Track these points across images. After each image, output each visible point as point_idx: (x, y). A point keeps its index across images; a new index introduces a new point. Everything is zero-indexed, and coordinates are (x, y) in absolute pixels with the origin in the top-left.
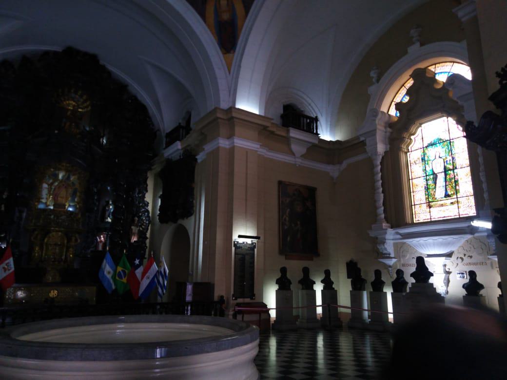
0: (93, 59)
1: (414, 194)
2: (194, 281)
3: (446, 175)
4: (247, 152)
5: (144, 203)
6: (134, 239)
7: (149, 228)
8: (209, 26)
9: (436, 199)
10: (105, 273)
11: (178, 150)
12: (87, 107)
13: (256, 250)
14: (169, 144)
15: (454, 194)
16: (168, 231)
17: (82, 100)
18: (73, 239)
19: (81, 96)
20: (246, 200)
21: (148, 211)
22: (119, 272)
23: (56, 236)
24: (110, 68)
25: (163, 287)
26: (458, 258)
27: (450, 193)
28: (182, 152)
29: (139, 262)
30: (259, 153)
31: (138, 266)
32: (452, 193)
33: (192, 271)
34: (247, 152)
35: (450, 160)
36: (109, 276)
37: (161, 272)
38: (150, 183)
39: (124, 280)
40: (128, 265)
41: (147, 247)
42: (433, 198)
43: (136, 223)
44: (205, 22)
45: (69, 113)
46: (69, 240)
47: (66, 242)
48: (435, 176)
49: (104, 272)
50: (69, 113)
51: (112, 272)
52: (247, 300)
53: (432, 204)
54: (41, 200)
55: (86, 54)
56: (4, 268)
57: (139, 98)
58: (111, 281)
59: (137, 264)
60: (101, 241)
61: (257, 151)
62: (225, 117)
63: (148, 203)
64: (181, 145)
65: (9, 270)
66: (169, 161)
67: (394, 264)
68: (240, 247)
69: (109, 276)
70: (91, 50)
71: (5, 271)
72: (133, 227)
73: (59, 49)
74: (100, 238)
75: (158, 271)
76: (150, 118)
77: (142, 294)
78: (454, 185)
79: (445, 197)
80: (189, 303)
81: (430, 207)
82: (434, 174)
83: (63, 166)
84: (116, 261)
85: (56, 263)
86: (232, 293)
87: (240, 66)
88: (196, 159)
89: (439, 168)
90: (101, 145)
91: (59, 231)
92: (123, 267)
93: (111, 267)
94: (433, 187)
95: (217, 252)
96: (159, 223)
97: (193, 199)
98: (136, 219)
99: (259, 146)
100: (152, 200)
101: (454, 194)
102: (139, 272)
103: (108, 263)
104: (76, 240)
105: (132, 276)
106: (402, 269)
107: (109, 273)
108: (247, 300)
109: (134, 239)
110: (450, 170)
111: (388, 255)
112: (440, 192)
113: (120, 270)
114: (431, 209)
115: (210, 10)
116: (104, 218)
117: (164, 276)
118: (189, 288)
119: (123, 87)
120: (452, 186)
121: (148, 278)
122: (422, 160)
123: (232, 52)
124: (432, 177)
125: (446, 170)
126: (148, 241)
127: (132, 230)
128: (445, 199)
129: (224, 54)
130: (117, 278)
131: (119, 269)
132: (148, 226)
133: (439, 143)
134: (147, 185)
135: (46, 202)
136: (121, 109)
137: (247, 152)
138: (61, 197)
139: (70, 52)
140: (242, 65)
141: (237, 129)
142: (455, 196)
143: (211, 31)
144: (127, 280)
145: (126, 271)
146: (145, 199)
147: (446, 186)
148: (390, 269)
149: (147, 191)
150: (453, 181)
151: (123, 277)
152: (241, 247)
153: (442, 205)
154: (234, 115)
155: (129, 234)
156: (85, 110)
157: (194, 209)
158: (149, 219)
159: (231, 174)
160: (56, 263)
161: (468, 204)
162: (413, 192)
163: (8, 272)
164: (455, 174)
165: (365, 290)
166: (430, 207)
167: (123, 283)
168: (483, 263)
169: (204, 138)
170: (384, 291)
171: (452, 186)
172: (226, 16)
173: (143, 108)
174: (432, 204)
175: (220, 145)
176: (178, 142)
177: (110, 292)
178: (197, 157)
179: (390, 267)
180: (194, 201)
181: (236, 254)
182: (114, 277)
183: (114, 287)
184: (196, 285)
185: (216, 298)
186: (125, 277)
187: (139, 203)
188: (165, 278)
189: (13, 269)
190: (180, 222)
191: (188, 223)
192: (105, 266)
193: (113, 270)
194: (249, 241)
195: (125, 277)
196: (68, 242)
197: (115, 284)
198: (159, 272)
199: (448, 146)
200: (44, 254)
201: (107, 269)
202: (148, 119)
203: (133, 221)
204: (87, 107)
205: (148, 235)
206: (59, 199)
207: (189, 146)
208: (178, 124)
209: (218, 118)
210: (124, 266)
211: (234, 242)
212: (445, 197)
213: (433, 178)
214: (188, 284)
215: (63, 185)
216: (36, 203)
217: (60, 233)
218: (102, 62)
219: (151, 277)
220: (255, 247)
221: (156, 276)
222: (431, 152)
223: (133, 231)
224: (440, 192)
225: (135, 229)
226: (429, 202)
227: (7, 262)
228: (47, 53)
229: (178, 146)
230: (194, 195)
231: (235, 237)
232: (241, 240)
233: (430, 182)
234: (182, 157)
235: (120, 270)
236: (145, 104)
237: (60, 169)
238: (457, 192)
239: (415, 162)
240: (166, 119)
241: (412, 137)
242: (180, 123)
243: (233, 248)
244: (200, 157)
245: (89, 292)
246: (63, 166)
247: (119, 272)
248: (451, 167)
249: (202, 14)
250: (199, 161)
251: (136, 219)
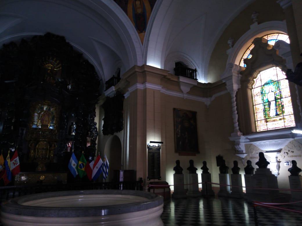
0: (63, 39)
1: (257, 114)
2: (125, 169)
3: (276, 102)
4: (154, 91)
5: (94, 124)
6: (89, 145)
7: (97, 138)
8: (130, 17)
9: (270, 117)
10: (72, 165)
11: (114, 91)
12: (59, 67)
13: (161, 150)
14: (107, 88)
15: (281, 114)
16: (109, 139)
17: (56, 64)
18: (53, 145)
19: (56, 61)
20: (154, 120)
21: (96, 128)
22: (80, 164)
23: (42, 144)
24: (72, 44)
25: (106, 173)
26: (285, 153)
27: (279, 113)
28: (115, 92)
29: (91, 158)
30: (161, 92)
31: (91, 161)
32: (280, 113)
33: (123, 163)
34: (154, 91)
35: (278, 93)
36: (74, 167)
37: (104, 164)
38: (97, 112)
39: (83, 169)
40: (85, 160)
41: (96, 149)
42: (268, 117)
43: (89, 135)
44: (127, 14)
45: (49, 71)
46: (51, 146)
47: (49, 147)
48: (269, 103)
49: (71, 165)
50: (49, 71)
51: (76, 164)
52: (156, 180)
53: (268, 120)
54: (34, 123)
55: (58, 36)
56: (13, 163)
57: (90, 61)
58: (76, 170)
59: (91, 160)
60: (69, 146)
61: (160, 91)
62: (141, 71)
63: (96, 123)
64: (115, 88)
65: (16, 164)
66: (108, 98)
67: (245, 157)
68: (151, 149)
69: (74, 167)
70: (61, 34)
71: (14, 165)
72: (87, 138)
73: (42, 34)
74: (69, 145)
75: (103, 164)
76: (96, 73)
77: (94, 177)
78: (281, 108)
79: (276, 115)
80: (121, 182)
81: (267, 122)
82: (269, 102)
83: (46, 102)
84: (78, 158)
85: (44, 159)
86: (147, 176)
87: (148, 40)
88: (124, 96)
89: (271, 97)
90: (67, 90)
91: (46, 141)
92: (82, 162)
93: (75, 162)
94: (269, 110)
95: (138, 152)
96: (103, 135)
97: (123, 120)
98: (89, 133)
99: (161, 88)
100: (98, 122)
101: (281, 114)
102: (91, 164)
103: (74, 160)
104: (55, 146)
105: (88, 167)
106: (250, 160)
107: (74, 165)
108: (156, 180)
109: (89, 145)
110: (278, 99)
111: (242, 152)
112: (272, 113)
113: (81, 163)
114: (268, 123)
115: (130, 7)
116: (70, 132)
117: (106, 166)
118: (122, 173)
119: (80, 55)
120: (280, 109)
121: (97, 168)
122: (261, 93)
123: (144, 32)
124: (267, 103)
125: (276, 99)
126: (96, 146)
127: (87, 139)
128: (276, 117)
129: (139, 33)
130: (79, 168)
131: (80, 163)
132: (97, 137)
133: (271, 83)
134: (95, 113)
135: (37, 124)
136: (79, 67)
137: (154, 91)
138: (45, 121)
139: (49, 35)
140: (150, 39)
141: (148, 78)
142: (282, 115)
143: (131, 20)
144: (85, 169)
145: (84, 164)
146: (95, 121)
147: (276, 109)
148: (243, 160)
149: (95, 116)
150: (281, 105)
151: (83, 167)
152: (152, 148)
153: (274, 121)
154: (146, 69)
155: (86, 142)
156: (59, 69)
157: (124, 125)
158: (97, 133)
159: (145, 104)
160: (44, 159)
161: (290, 120)
162: (256, 113)
163: (16, 166)
164: (282, 101)
165: (228, 173)
166: (267, 122)
167: (82, 171)
168: (300, 155)
169: (128, 84)
170: (240, 173)
171: (280, 109)
172: (139, 11)
173: (92, 67)
174: (268, 120)
175: (138, 87)
176: (113, 86)
177: (75, 176)
178: (125, 95)
179: (243, 159)
180: (123, 122)
181: (149, 152)
182: (77, 168)
183: (77, 173)
184: (125, 172)
185: (137, 179)
186: (83, 168)
187: (91, 123)
188: (107, 168)
189: (19, 164)
190: (115, 134)
191: (120, 135)
192: (72, 160)
193: (76, 163)
194: (157, 145)
195: (83, 168)
196: (49, 148)
197: (78, 172)
198: (103, 164)
199: (277, 84)
200: (36, 155)
201: (73, 163)
202: (95, 73)
203: (88, 134)
204: (59, 67)
205: (97, 142)
206: (44, 122)
207: (119, 88)
208: (112, 76)
209: (136, 71)
210: (83, 161)
211: (148, 145)
212: (276, 115)
213: (268, 104)
214: (120, 171)
215: (47, 114)
216: (31, 125)
217: (45, 142)
218: (67, 41)
219: (99, 167)
220: (160, 148)
221: (101, 166)
222: (267, 88)
223: (88, 140)
224: (272, 113)
225: (89, 139)
226: (266, 119)
227: (15, 159)
228: (36, 37)
229: (113, 89)
230: (123, 118)
231: (148, 143)
232: (152, 144)
233: (267, 107)
234: (115, 96)
235: (81, 163)
236: (94, 65)
237: (44, 105)
238: (283, 112)
239: (257, 95)
240: (105, 73)
241: (255, 80)
242: (114, 75)
243: (147, 149)
244: (126, 95)
245: (63, 177)
246: (46, 102)
247: (80, 164)
248: (279, 97)
249: (126, 11)
250: (126, 97)
251: (89, 133)
